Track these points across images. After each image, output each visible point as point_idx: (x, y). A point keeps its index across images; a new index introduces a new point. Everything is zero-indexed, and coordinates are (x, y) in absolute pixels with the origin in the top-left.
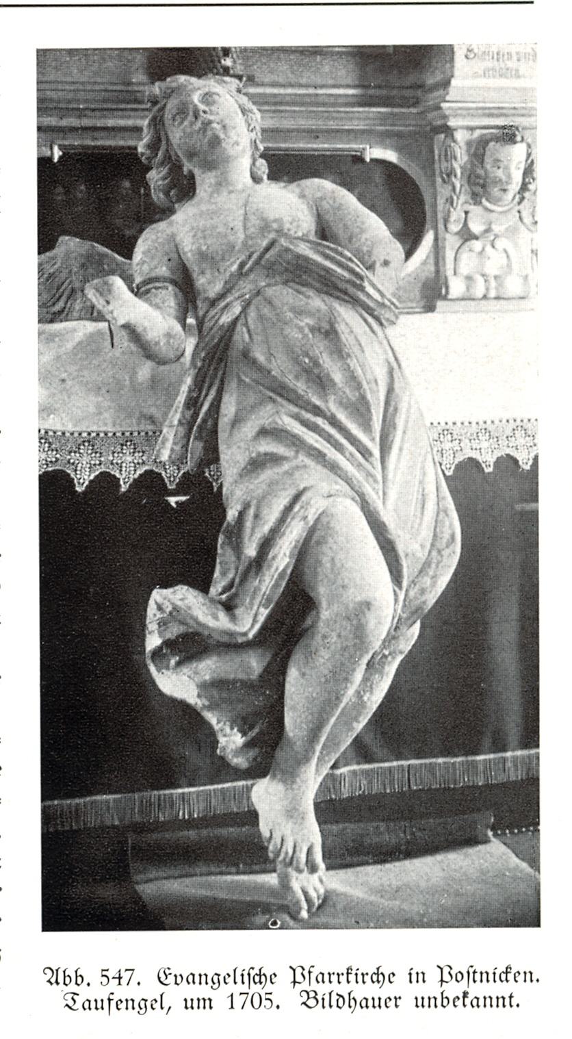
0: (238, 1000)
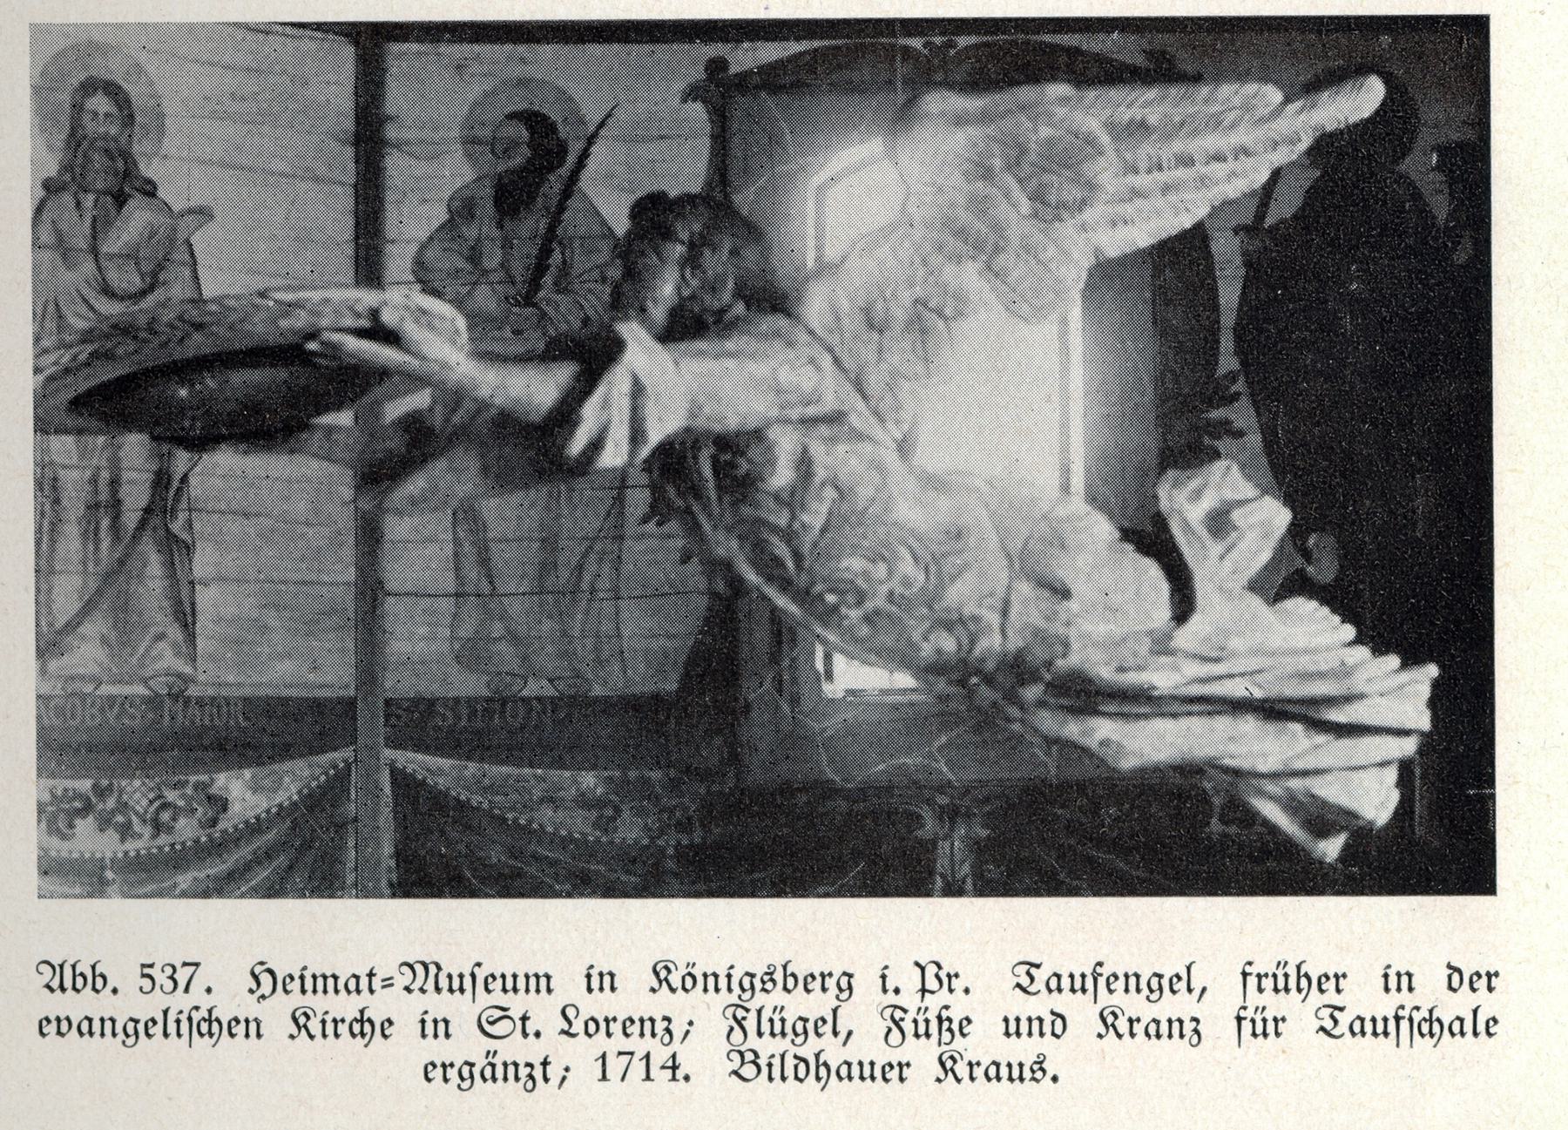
0: (615, 1066)
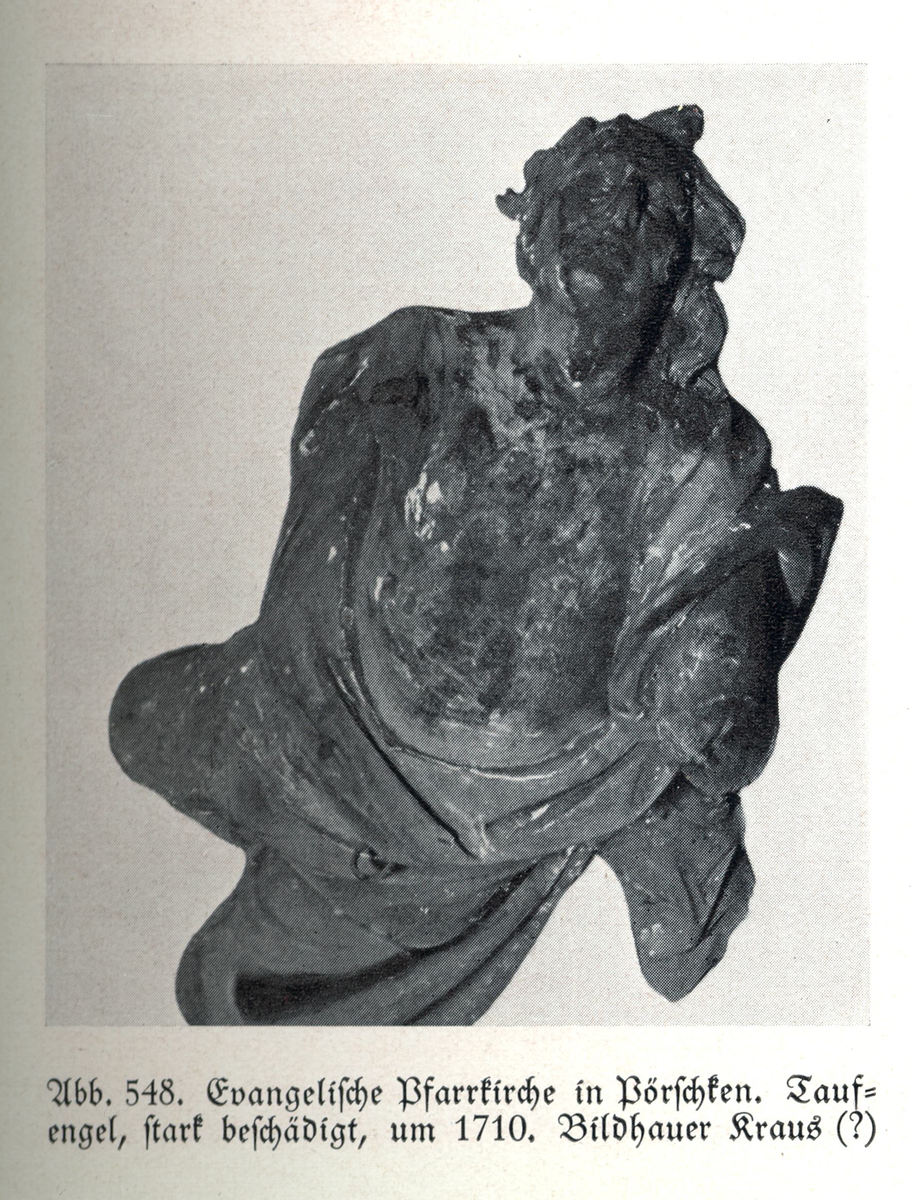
0: (473, 1127)
